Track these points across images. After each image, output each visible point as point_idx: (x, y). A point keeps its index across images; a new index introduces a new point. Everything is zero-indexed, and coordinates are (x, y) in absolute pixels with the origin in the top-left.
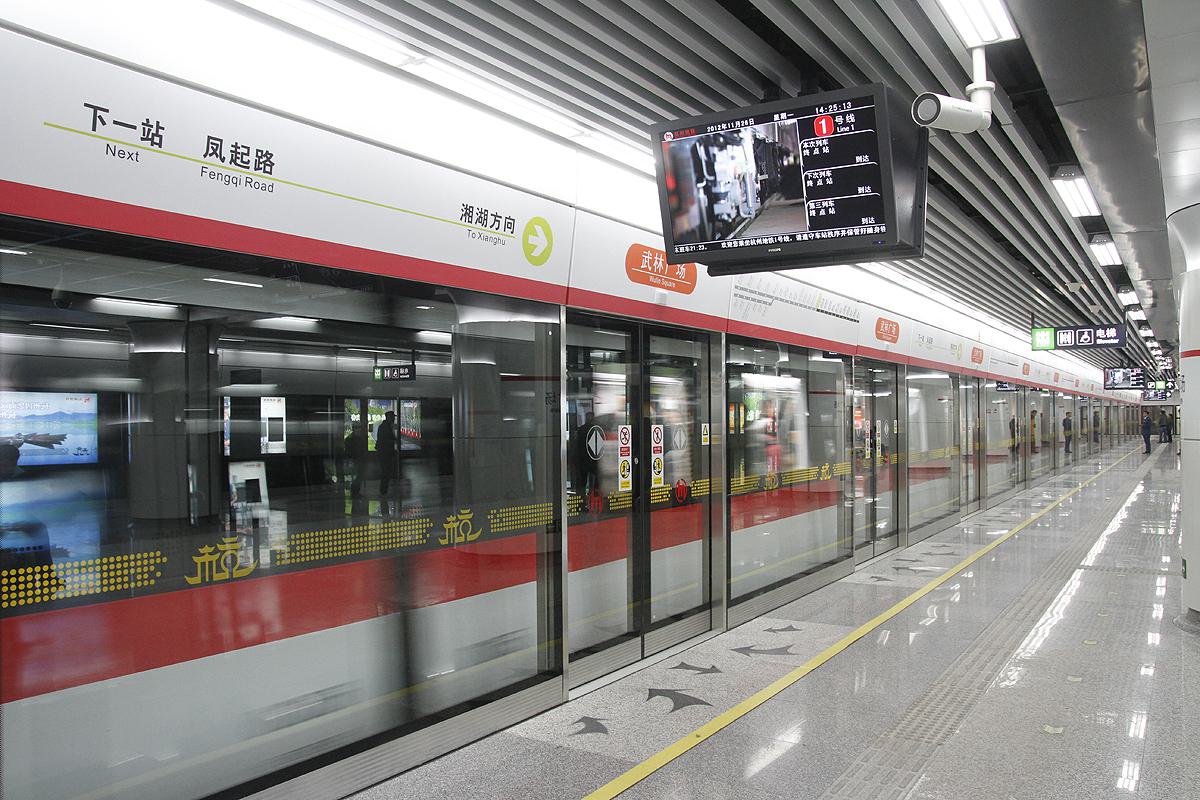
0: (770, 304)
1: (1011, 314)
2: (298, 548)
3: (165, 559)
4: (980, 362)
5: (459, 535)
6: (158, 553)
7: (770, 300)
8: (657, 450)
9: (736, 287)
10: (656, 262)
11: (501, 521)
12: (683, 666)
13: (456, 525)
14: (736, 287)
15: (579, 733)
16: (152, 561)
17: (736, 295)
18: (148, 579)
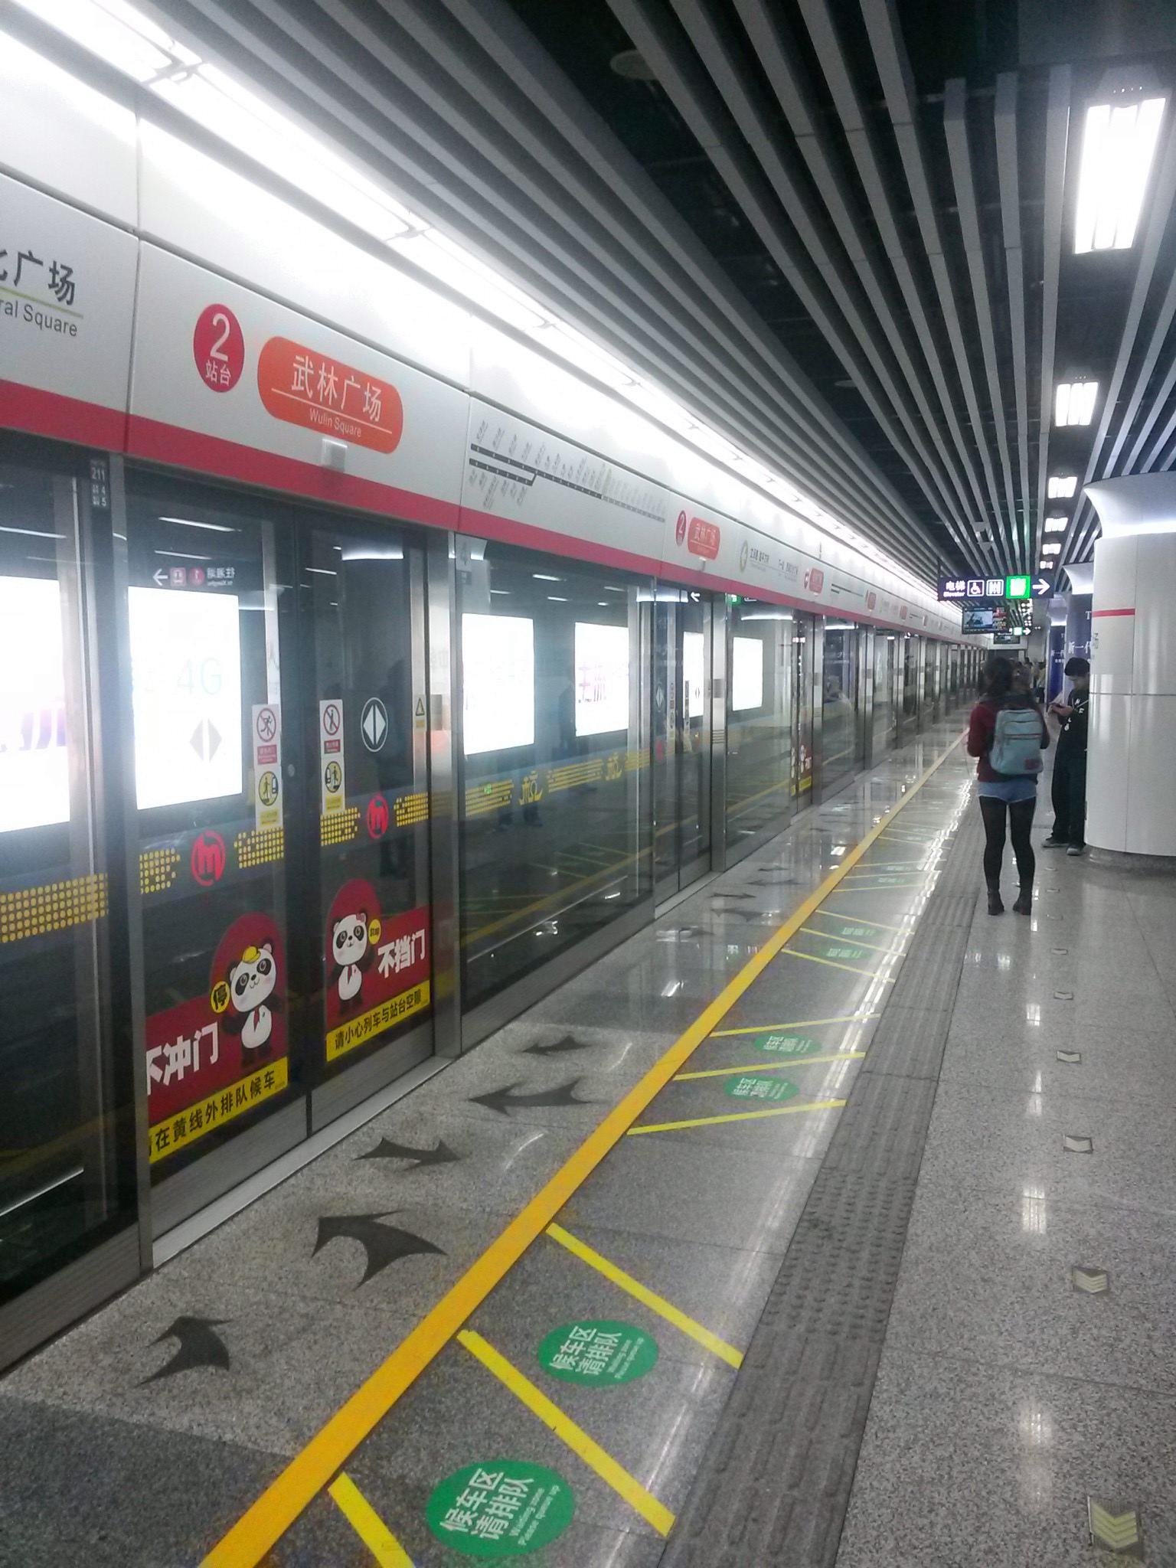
0: (530, 483)
1: (877, 509)
4: (819, 591)
7: (529, 476)
8: (332, 747)
9: (474, 447)
10: (322, 382)
11: (253, 849)
14: (474, 447)
17: (472, 462)
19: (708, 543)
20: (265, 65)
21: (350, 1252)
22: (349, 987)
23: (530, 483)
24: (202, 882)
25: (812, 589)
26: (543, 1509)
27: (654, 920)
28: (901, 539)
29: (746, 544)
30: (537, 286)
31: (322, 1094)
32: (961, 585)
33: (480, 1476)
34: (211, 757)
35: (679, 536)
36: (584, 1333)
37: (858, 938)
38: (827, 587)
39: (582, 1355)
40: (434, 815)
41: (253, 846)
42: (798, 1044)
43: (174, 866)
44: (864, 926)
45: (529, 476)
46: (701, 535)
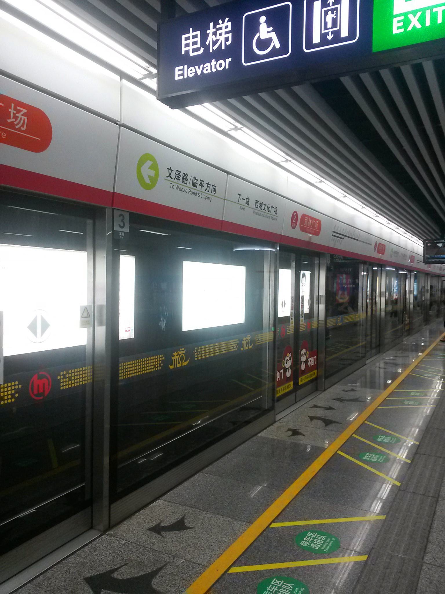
0: (343, 239)
2: (73, 378)
3: (59, 378)
5: (179, 363)
6: (17, 383)
7: (343, 237)
11: (200, 354)
12: (315, 406)
13: (177, 357)
15: (116, 569)
16: (13, 388)
18: (11, 399)
19: (313, 227)
20: (103, 13)
21: (290, 433)
22: (303, 367)
23: (343, 239)
24: (35, 397)
25: (379, 252)
26: (331, 543)
27: (275, 422)
28: (374, 188)
29: (392, 249)
30: (142, 48)
31: (299, 392)
32: (221, 33)
33: (275, 581)
34: (41, 335)
35: (375, 248)
36: (278, 582)
37: (432, 372)
38: (416, 261)
39: (312, 542)
40: (95, 379)
41: (70, 379)
42: (379, 458)
43: (17, 391)
44: (390, 435)
45: (343, 237)
46: (381, 247)
